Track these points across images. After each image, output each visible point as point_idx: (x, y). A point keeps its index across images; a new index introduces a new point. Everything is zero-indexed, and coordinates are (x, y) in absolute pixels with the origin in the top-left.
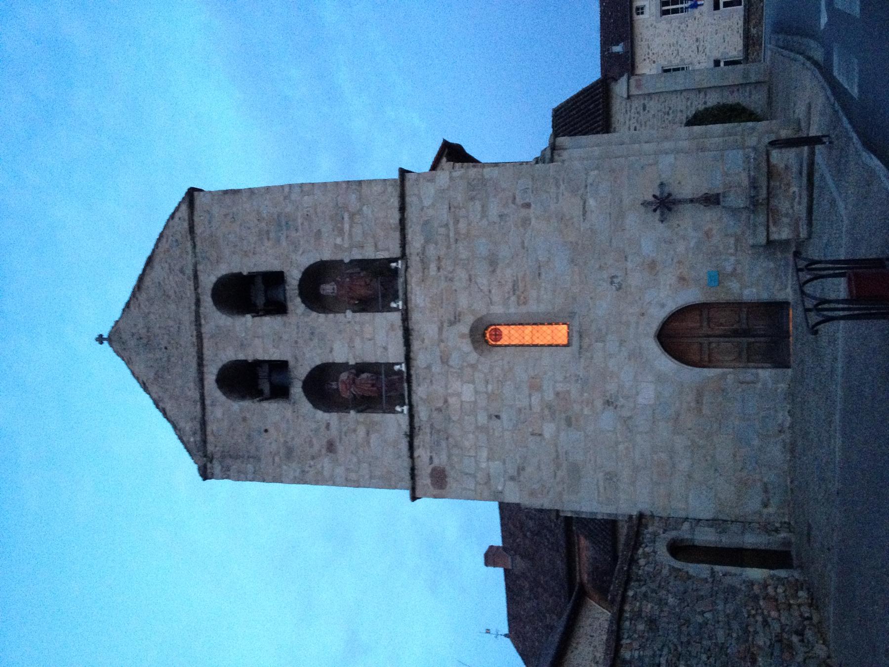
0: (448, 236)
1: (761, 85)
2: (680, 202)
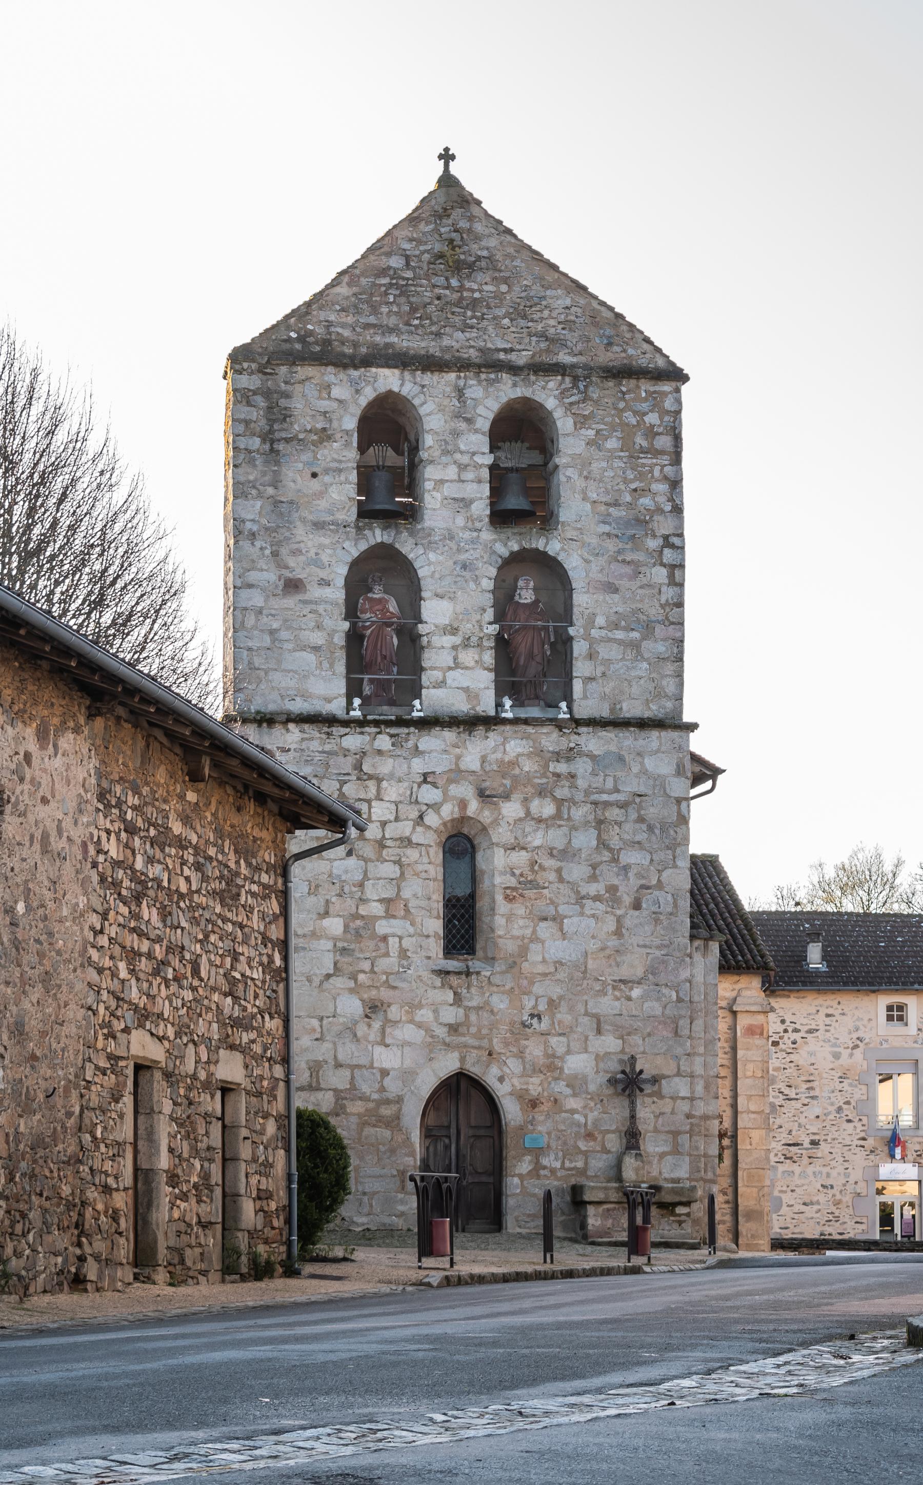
0: (602, 792)
1: (752, 1215)
2: (633, 1104)
